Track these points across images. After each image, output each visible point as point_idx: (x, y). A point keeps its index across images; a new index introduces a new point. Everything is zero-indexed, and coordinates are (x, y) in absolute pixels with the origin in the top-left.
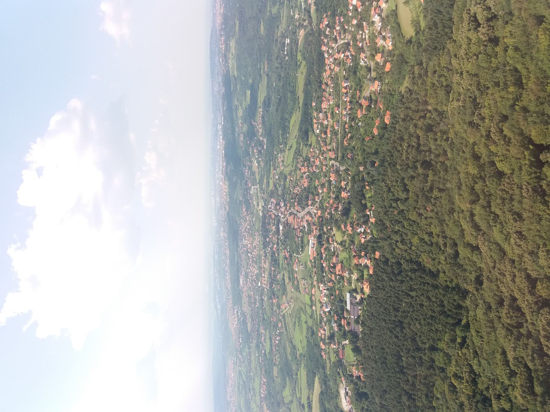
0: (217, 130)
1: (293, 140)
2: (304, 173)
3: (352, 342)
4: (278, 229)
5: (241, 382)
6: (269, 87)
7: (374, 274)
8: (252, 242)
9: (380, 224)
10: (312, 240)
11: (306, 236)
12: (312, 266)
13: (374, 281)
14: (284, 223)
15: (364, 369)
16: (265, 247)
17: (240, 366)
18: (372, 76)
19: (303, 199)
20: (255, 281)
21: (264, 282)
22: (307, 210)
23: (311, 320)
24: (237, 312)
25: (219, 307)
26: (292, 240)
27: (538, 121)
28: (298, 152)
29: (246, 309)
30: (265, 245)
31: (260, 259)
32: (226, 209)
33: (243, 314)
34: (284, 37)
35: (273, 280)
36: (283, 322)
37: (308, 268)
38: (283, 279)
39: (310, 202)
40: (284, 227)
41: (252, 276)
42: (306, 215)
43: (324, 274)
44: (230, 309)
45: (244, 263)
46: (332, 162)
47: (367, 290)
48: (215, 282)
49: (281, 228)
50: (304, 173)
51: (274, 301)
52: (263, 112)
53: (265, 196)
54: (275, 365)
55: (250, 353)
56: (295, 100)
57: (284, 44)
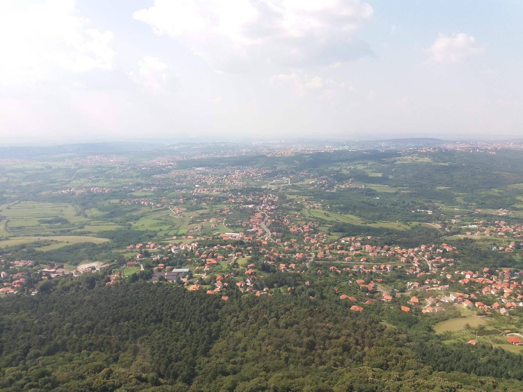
0: (343, 145)
2: (303, 229)
3: (142, 273)
4: (250, 203)
5: (104, 169)
7: (206, 295)
8: (237, 179)
10: (238, 236)
12: (215, 236)
14: (255, 209)
15: (116, 285)
16: (232, 191)
17: (120, 168)
22: (268, 231)
28: (322, 222)
30: (234, 191)
31: (221, 186)
33: (169, 171)
34: (434, 208)
36: (161, 208)
38: (202, 209)
39: (275, 233)
41: (204, 179)
43: (206, 247)
46: (313, 255)
51: (181, 200)
52: (362, 189)
54: (121, 201)
55: (132, 177)
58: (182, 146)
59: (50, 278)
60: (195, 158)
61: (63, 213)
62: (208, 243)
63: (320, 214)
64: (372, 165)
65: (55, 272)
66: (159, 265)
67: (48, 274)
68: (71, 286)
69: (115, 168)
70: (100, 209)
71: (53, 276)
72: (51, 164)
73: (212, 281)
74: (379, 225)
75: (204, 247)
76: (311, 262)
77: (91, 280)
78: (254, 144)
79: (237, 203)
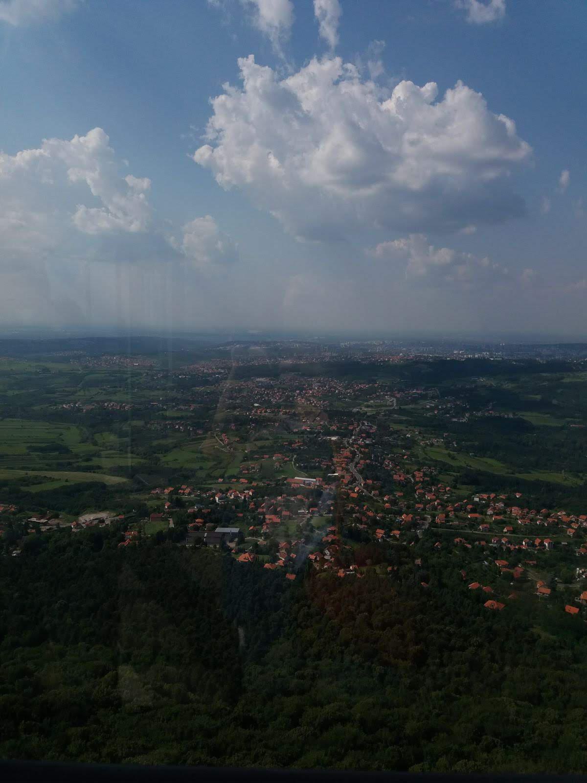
1: (463, 461)
2: (414, 476)
3: (171, 531)
14: (342, 443)
18: (559, 585)
22: (359, 477)
24: (220, 373)
28: (445, 468)
39: (370, 482)
50: (414, 476)
54: (146, 423)
59: (39, 531)
71: (44, 529)
72: (49, 365)
75: (263, 497)
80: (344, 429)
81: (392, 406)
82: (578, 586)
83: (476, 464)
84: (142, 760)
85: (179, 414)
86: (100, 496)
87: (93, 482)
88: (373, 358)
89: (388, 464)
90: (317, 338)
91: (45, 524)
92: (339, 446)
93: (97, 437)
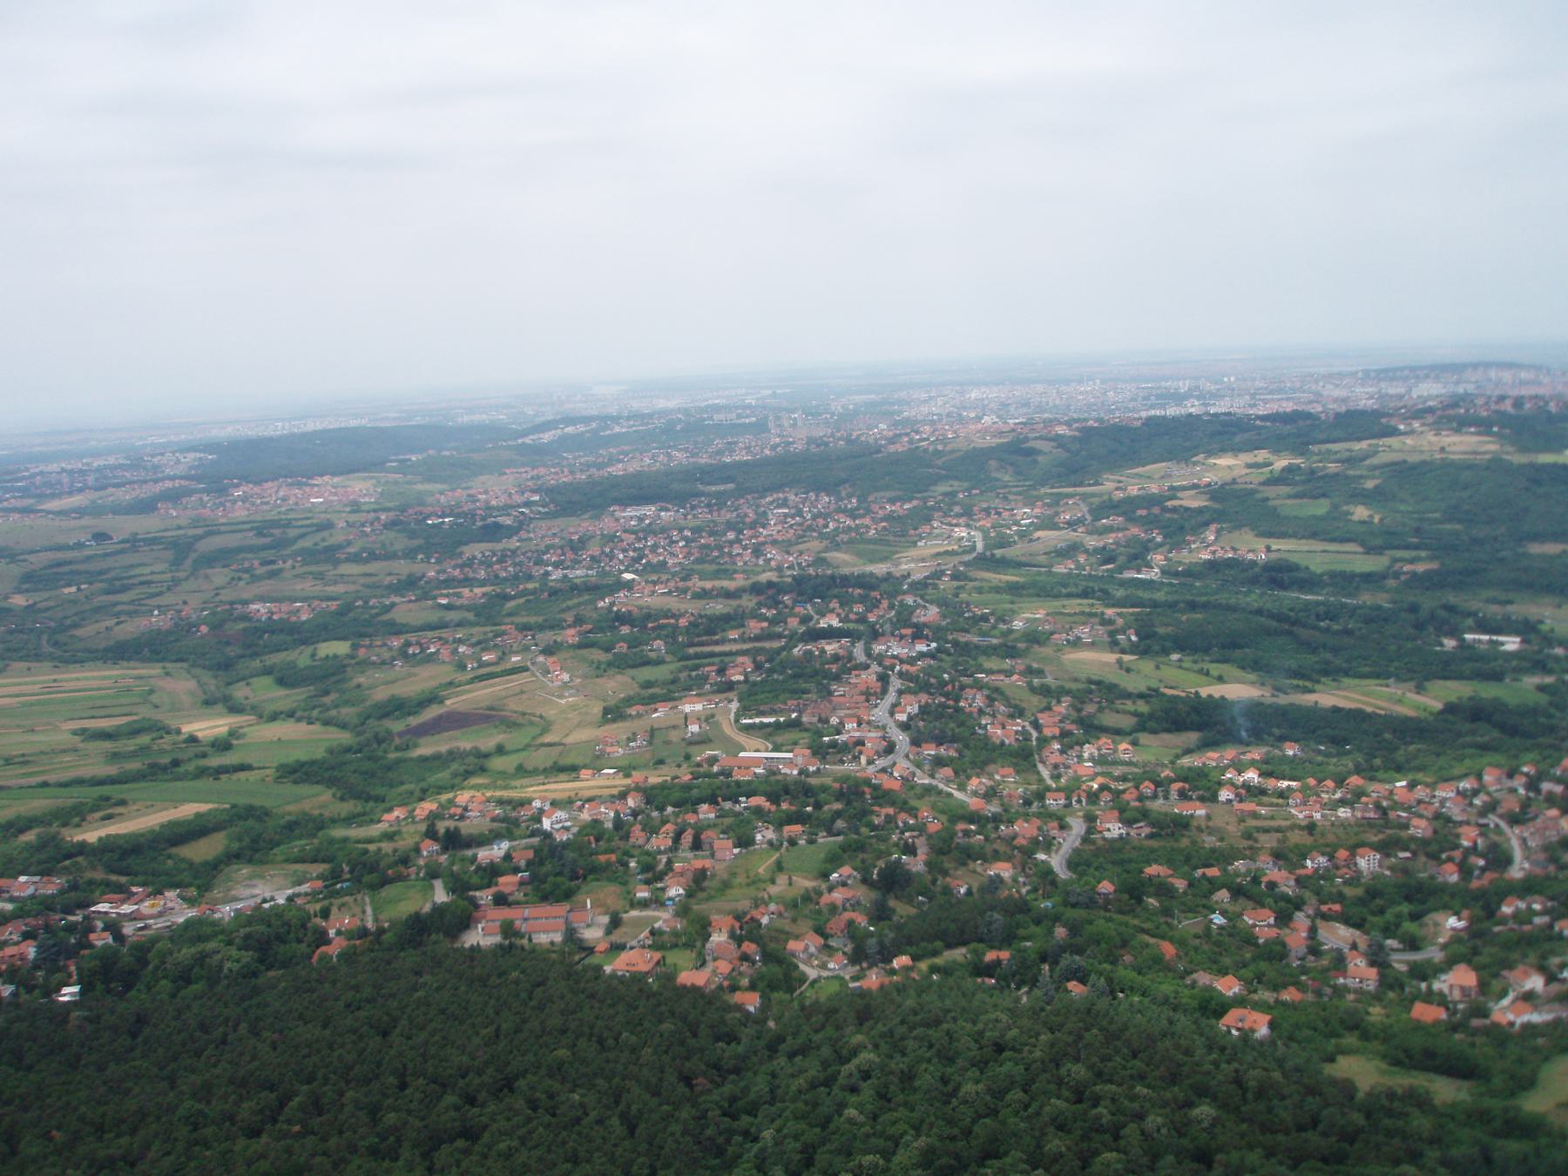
0: (1179, 398)
1: (1145, 674)
2: (1036, 725)
3: (439, 910)
4: (830, 634)
5: (292, 533)
6: (1346, 581)
7: (676, 988)
8: (779, 540)
9: (864, 1009)
10: (791, 761)
11: (805, 738)
12: (699, 765)
13: (654, 999)
14: (850, 658)
15: (348, 957)
16: (756, 589)
17: (349, 525)
18: (1395, 956)
19: (944, 726)
20: (637, 560)
21: (647, 597)
22: (901, 738)
23: (511, 769)
24: (527, 504)
25: (547, 437)
26: (789, 683)
27: (881, 814)
28: (1109, 692)
29: (544, 533)
30: (768, 592)
31: (717, 575)
32: (892, 441)
33: (521, 525)
34: (1526, 629)
35: (644, 621)
36: (498, 669)
37: (693, 750)
38: (647, 663)
39: (930, 751)
40: (836, 658)
41: (654, 548)
42: (876, 732)
43: (670, 809)
44: (539, 478)
45: (703, 516)
46: (1078, 826)
47: (616, 966)
48: (628, 418)
49: (831, 648)
50: (1036, 725)
51: (572, 631)
52: (1253, 563)
53: (946, 583)
54: (355, 647)
55: (392, 556)
56: (1307, 676)
57: (1499, 632)
58: (570, 429)
59: (119, 937)
60: (617, 470)
61: (154, 698)
62: (676, 795)
63: (1096, 661)
64: (1289, 470)
65: (155, 913)
66: (502, 880)
67: (113, 927)
68: (185, 964)
69: (329, 526)
70: (281, 682)
71: (128, 929)
72: (106, 523)
73: (696, 934)
74: (1326, 697)
75: (661, 809)
76: (669, 977)
77: (273, 938)
78: (837, 407)
79: (780, 636)
80: (857, 621)
81: (973, 548)
82: (1434, 954)
83: (1181, 678)
84: (355, 832)
85: (434, 617)
86: (256, 839)
87: (293, 435)
88: (917, 432)
89: (974, 700)
90: (769, 392)
91: (133, 917)
92: (847, 665)
93: (240, 692)
